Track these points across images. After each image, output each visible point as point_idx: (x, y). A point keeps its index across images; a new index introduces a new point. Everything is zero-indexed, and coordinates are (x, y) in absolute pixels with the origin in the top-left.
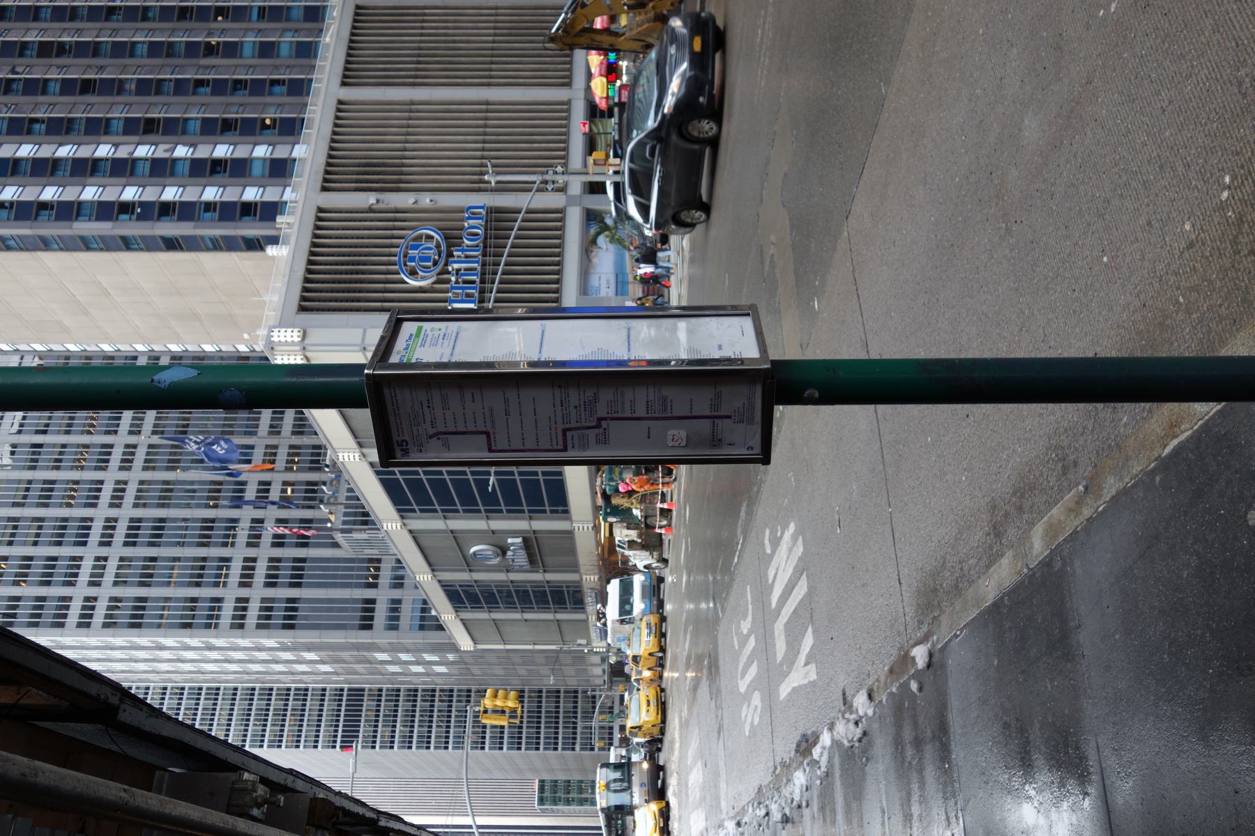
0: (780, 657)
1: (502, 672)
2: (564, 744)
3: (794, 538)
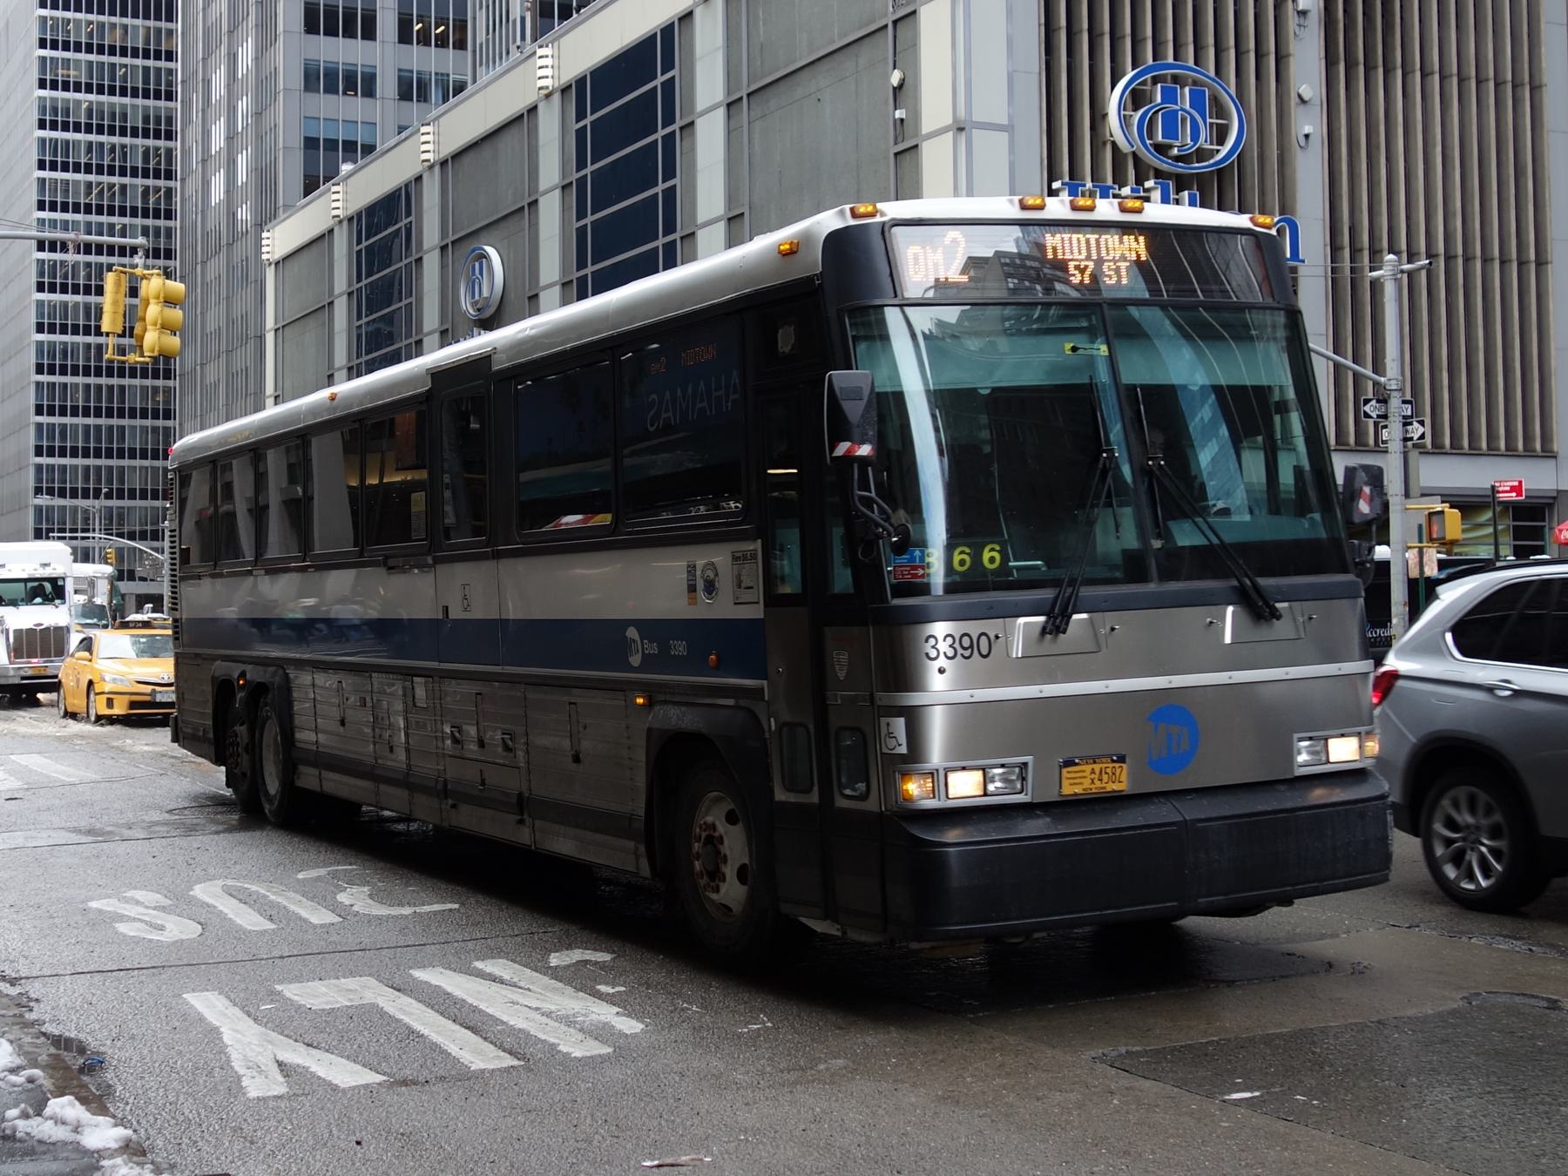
0: (291, 991)
1: (211, 326)
2: (51, 468)
3: (601, 1032)
